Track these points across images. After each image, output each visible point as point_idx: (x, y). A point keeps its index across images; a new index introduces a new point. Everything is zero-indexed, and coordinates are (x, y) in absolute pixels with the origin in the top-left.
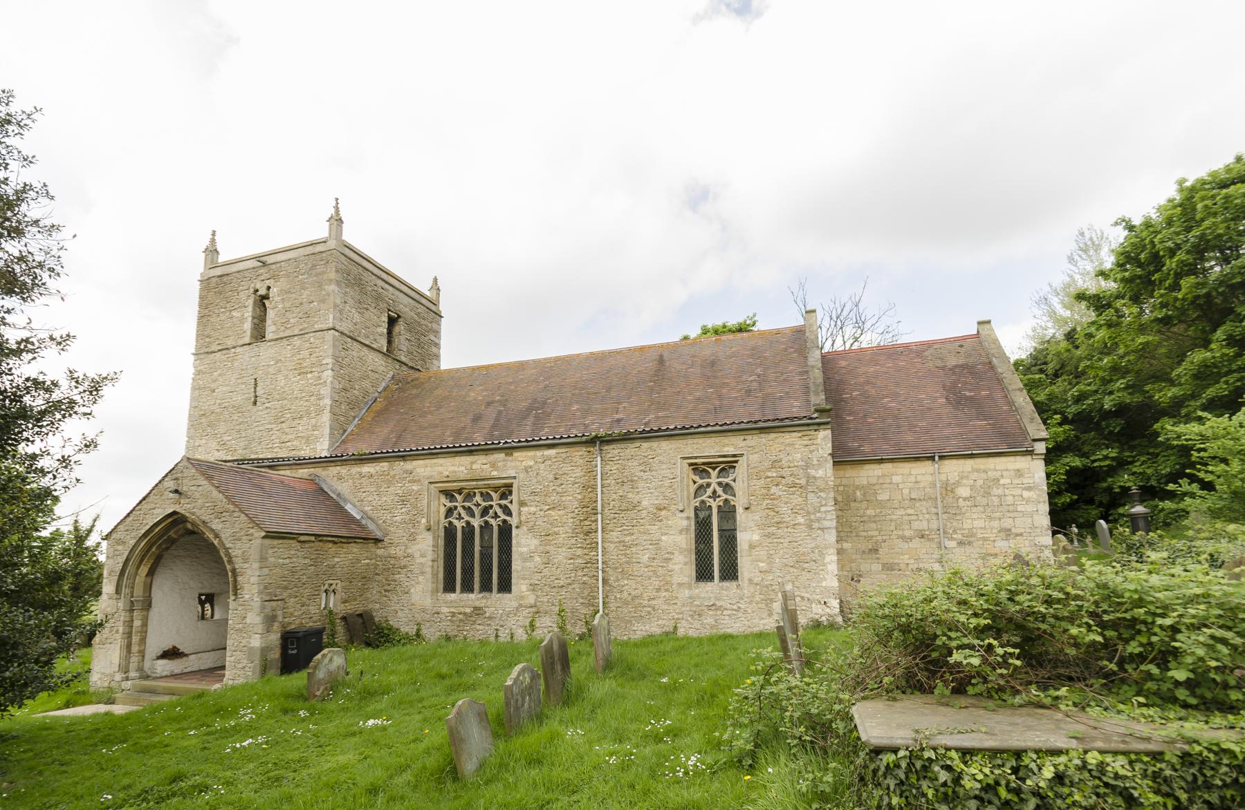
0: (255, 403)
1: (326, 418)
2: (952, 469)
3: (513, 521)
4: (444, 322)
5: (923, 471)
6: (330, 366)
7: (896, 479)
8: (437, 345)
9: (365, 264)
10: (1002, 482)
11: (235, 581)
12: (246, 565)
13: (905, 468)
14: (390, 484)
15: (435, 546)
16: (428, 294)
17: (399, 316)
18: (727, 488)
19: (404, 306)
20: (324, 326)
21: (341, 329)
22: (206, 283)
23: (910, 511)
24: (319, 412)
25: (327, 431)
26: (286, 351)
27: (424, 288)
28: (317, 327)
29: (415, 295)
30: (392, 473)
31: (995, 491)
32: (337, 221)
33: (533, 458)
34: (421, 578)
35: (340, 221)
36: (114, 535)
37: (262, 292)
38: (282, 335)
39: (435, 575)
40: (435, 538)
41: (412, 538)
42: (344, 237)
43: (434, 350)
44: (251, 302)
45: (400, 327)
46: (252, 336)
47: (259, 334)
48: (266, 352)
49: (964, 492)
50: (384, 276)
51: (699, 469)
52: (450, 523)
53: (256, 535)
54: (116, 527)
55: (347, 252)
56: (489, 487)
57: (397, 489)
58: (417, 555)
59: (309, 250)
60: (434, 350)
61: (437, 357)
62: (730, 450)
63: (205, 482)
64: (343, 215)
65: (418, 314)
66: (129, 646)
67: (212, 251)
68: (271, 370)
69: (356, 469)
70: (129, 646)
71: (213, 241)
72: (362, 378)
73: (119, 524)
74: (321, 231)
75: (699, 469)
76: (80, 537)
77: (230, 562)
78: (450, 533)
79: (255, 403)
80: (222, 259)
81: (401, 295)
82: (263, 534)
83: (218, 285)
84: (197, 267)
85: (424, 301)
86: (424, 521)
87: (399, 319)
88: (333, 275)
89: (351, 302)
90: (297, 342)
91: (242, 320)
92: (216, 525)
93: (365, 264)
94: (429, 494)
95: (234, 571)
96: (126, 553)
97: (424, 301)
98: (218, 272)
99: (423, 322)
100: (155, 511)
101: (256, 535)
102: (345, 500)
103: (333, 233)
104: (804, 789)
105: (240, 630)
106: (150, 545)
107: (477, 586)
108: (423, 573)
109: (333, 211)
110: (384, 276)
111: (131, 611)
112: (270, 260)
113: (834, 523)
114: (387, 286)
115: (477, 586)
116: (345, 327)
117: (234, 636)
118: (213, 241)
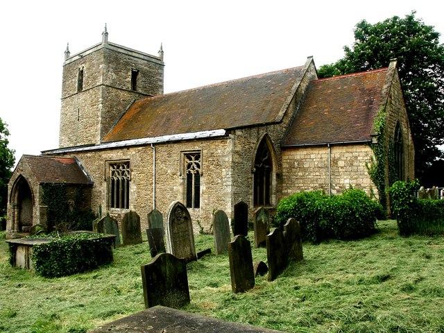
1: (99, 126)
2: (337, 152)
3: (200, 171)
4: (165, 68)
5: (323, 153)
7: (313, 156)
8: (162, 81)
10: (359, 158)
13: (316, 151)
18: (198, 166)
19: (142, 65)
23: (317, 174)
25: (100, 132)
28: (98, 84)
29: (149, 59)
31: (355, 164)
33: (135, 151)
35: (107, 34)
37: (81, 69)
39: (184, 194)
43: (160, 83)
44: (77, 75)
48: (82, 96)
49: (341, 163)
50: (130, 53)
51: (188, 156)
52: (189, 172)
56: (191, 154)
59: (96, 49)
60: (160, 83)
61: (162, 87)
62: (197, 148)
65: (150, 67)
66: (14, 221)
70: (14, 221)
74: (99, 39)
75: (188, 156)
78: (189, 175)
80: (71, 55)
84: (61, 60)
85: (153, 60)
89: (111, 70)
97: (153, 60)
102: (83, 168)
107: (115, 206)
110: (130, 53)
111: (14, 209)
112: (84, 54)
113: (231, 183)
114: (131, 58)
115: (115, 206)
116: (108, 83)
118: (68, 49)
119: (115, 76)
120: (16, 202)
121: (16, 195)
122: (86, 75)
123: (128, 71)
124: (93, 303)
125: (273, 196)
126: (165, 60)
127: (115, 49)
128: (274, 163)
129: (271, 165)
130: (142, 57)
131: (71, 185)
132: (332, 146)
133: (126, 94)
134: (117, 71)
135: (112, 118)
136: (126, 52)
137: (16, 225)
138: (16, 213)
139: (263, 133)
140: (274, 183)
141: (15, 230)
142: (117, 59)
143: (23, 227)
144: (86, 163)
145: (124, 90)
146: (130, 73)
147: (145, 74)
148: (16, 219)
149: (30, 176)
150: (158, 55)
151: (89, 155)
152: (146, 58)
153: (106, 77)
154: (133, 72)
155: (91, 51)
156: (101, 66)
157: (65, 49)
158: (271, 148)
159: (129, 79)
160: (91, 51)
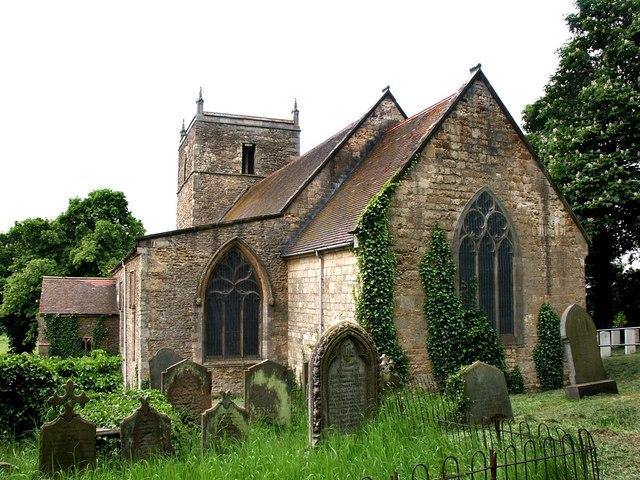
17: (254, 145)
19: (260, 136)
29: (272, 125)
50: (239, 122)
65: (274, 137)
85: (280, 126)
110: (239, 122)
116: (203, 168)
119: (214, 158)
123: (236, 147)
125: (265, 342)
126: (302, 124)
127: (214, 120)
128: (263, 287)
129: (258, 288)
131: (88, 316)
132: (322, 254)
133: (234, 181)
134: (216, 150)
136: (233, 122)
139: (226, 237)
140: (266, 319)
142: (217, 134)
145: (230, 175)
146: (240, 150)
147: (265, 148)
150: (290, 117)
152: (266, 124)
153: (200, 160)
154: (244, 148)
155: (226, 121)
158: (254, 261)
159: (239, 158)
160: (226, 121)
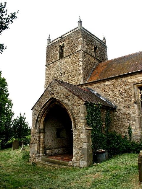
0: (61, 76)
1: (81, 76)
4: (107, 48)
6: (81, 61)
9: (87, 32)
11: (75, 122)
12: (79, 115)
14: (117, 87)
15: (139, 109)
16: (102, 40)
17: (97, 47)
20: (79, 50)
21: (84, 50)
22: (48, 47)
24: (79, 74)
26: (69, 59)
27: (102, 39)
30: (117, 83)
32: (80, 22)
34: (134, 123)
35: (81, 22)
36: (34, 108)
38: (67, 55)
40: (138, 106)
41: (128, 107)
42: (82, 26)
44: (59, 49)
45: (98, 50)
46: (60, 58)
47: (61, 57)
48: (63, 61)
50: (92, 36)
53: (82, 103)
54: (35, 105)
55: (83, 30)
57: (120, 89)
58: (131, 113)
59: (73, 31)
63: (61, 86)
64: (81, 20)
65: (101, 46)
66: (40, 145)
67: (49, 39)
68: (65, 65)
69: (102, 84)
71: (49, 37)
72: (89, 65)
73: (35, 104)
74: (76, 25)
76: (21, 118)
77: (72, 114)
79: (61, 76)
80: (51, 41)
81: (97, 41)
82: (84, 103)
83: (50, 48)
84: (46, 43)
85: (102, 43)
86: (133, 99)
87: (95, 47)
88: (80, 35)
90: (71, 56)
91: (57, 54)
92: (66, 101)
93: (87, 32)
94: (134, 89)
95: (74, 118)
96: (38, 114)
97: (102, 43)
98: (51, 44)
99: (103, 49)
100: (46, 99)
101: (82, 103)
102: (100, 96)
103: (80, 26)
104: (12, 127)
105: (77, 141)
106: (45, 110)
108: (135, 120)
109: (79, 20)
110: (92, 36)
111: (40, 133)
112: (63, 37)
114: (93, 39)
116: (84, 49)
117: (76, 143)
118: (49, 37)
120: (42, 126)
121: (43, 119)
122: (66, 47)
123: (92, 45)
124: (41, 173)
130: (98, 40)
134: (88, 44)
135: (88, 72)
137: (41, 149)
138: (42, 137)
141: (41, 155)
143: (48, 151)
144: (103, 91)
146: (93, 47)
148: (41, 143)
149: (67, 97)
151: (106, 83)
156: (79, 39)
157: (48, 38)
